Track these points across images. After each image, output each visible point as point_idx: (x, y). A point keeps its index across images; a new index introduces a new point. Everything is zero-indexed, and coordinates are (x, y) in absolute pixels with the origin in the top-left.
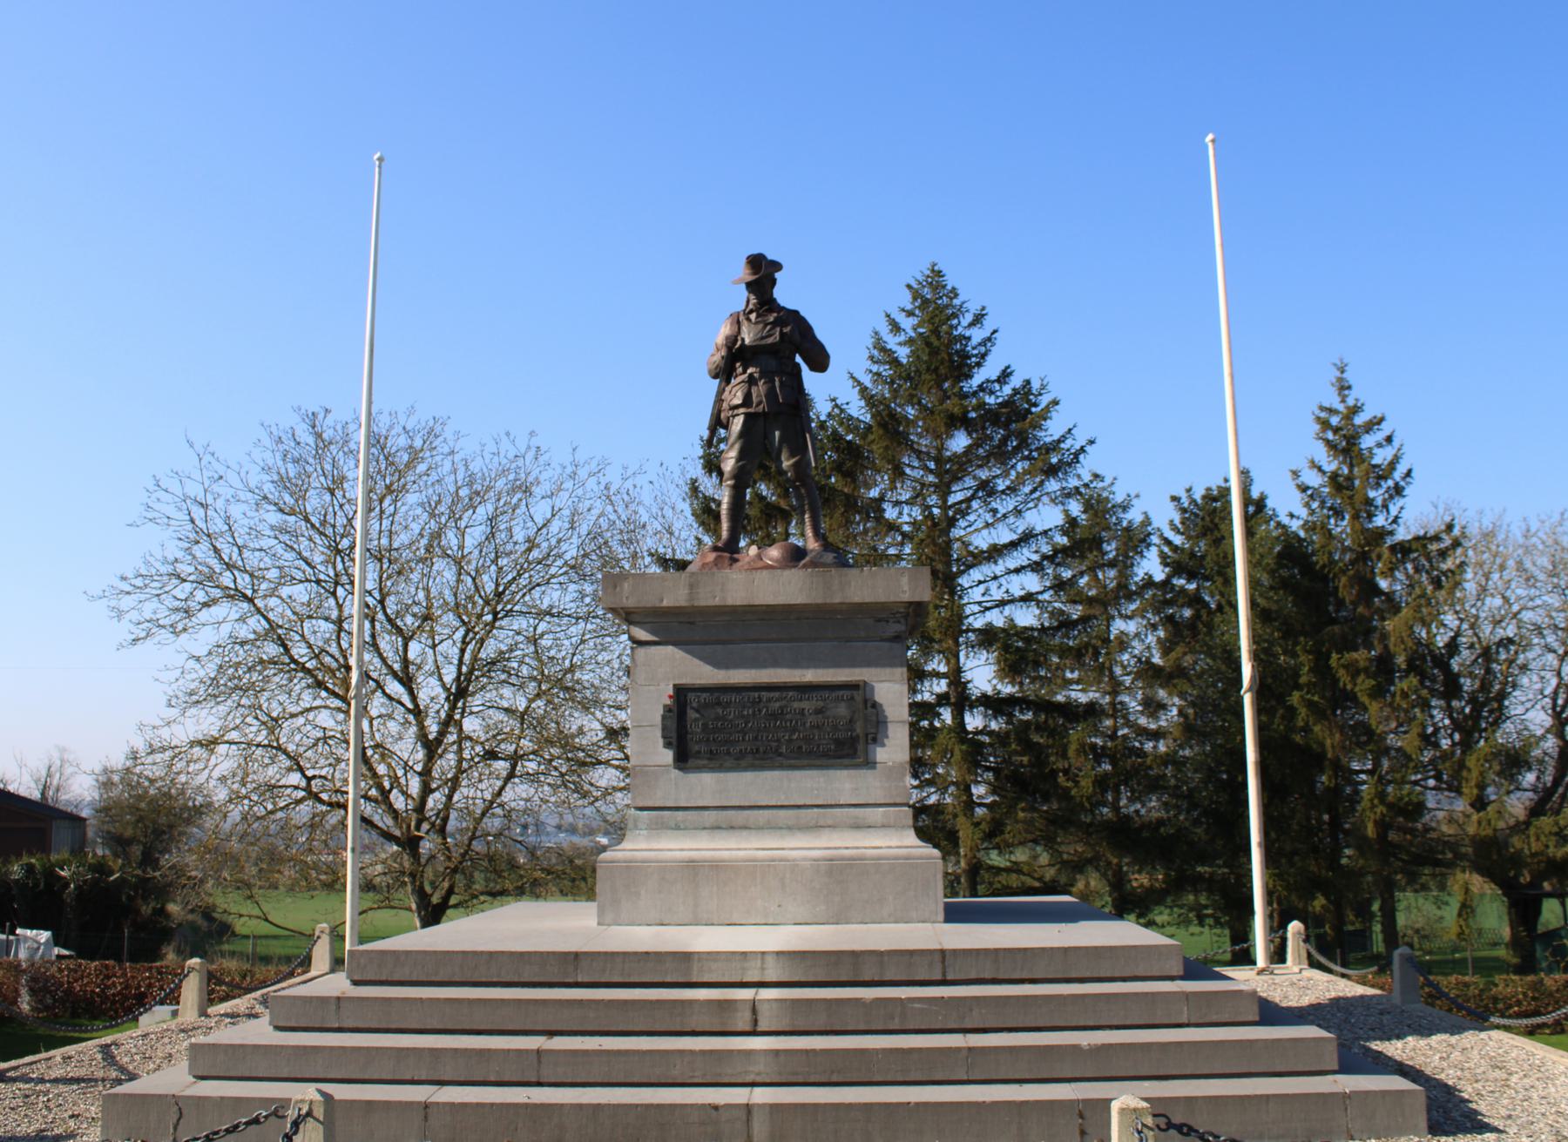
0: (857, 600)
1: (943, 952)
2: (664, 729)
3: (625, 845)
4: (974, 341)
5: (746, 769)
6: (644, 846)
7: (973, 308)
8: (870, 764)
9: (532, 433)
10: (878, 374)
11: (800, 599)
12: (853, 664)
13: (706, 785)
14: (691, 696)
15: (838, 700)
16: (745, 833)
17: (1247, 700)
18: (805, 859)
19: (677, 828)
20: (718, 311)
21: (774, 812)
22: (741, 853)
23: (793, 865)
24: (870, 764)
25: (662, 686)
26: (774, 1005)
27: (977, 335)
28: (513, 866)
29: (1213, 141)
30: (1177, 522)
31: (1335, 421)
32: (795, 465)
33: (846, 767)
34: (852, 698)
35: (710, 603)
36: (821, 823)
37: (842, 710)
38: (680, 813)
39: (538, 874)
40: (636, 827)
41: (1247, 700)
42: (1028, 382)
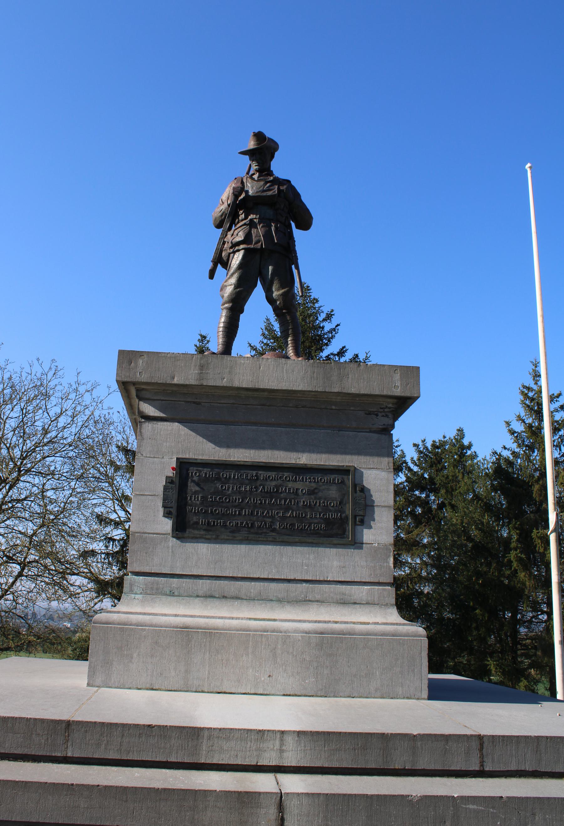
0: (353, 391)
1: (480, 738)
2: (165, 499)
3: (122, 607)
4: (326, 329)
5: (241, 542)
6: (139, 610)
7: (326, 310)
8: (357, 544)
9: (53, 361)
10: (267, 345)
11: (300, 386)
12: (345, 451)
13: (202, 555)
14: (193, 470)
15: (329, 483)
16: (236, 603)
17: (553, 538)
18: (296, 631)
19: (172, 594)
20: (227, 175)
21: (266, 584)
22: (235, 622)
23: (285, 637)
24: (357, 544)
25: (166, 459)
26: (305, 801)
27: (328, 326)
28: (18, 633)
29: (530, 167)
30: (415, 459)
31: (531, 394)
32: (283, 295)
33: (335, 546)
34: (343, 482)
35: (219, 383)
36: (310, 597)
37: (333, 493)
38: (175, 580)
39: (32, 638)
40: (131, 591)
41: (553, 538)
42: (357, 356)
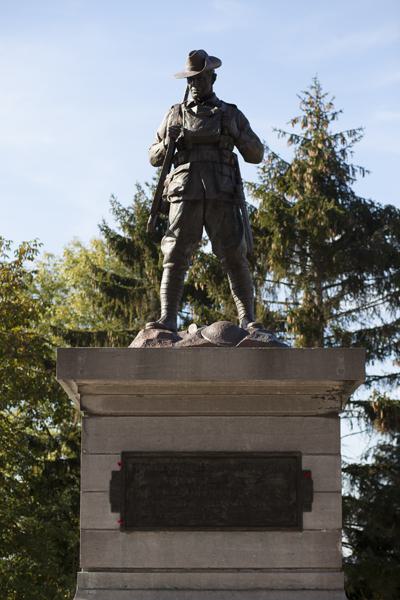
20: (165, 97)
